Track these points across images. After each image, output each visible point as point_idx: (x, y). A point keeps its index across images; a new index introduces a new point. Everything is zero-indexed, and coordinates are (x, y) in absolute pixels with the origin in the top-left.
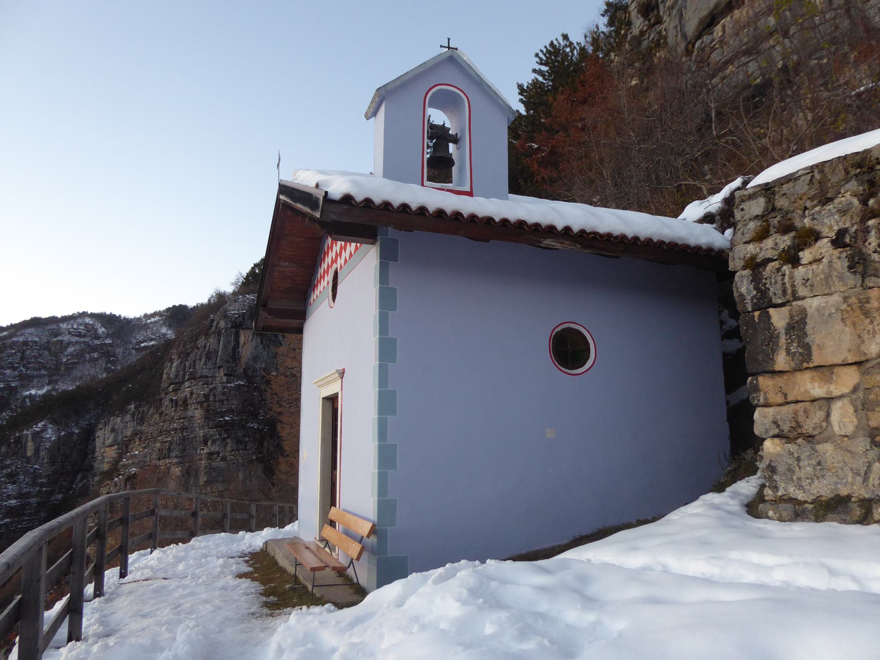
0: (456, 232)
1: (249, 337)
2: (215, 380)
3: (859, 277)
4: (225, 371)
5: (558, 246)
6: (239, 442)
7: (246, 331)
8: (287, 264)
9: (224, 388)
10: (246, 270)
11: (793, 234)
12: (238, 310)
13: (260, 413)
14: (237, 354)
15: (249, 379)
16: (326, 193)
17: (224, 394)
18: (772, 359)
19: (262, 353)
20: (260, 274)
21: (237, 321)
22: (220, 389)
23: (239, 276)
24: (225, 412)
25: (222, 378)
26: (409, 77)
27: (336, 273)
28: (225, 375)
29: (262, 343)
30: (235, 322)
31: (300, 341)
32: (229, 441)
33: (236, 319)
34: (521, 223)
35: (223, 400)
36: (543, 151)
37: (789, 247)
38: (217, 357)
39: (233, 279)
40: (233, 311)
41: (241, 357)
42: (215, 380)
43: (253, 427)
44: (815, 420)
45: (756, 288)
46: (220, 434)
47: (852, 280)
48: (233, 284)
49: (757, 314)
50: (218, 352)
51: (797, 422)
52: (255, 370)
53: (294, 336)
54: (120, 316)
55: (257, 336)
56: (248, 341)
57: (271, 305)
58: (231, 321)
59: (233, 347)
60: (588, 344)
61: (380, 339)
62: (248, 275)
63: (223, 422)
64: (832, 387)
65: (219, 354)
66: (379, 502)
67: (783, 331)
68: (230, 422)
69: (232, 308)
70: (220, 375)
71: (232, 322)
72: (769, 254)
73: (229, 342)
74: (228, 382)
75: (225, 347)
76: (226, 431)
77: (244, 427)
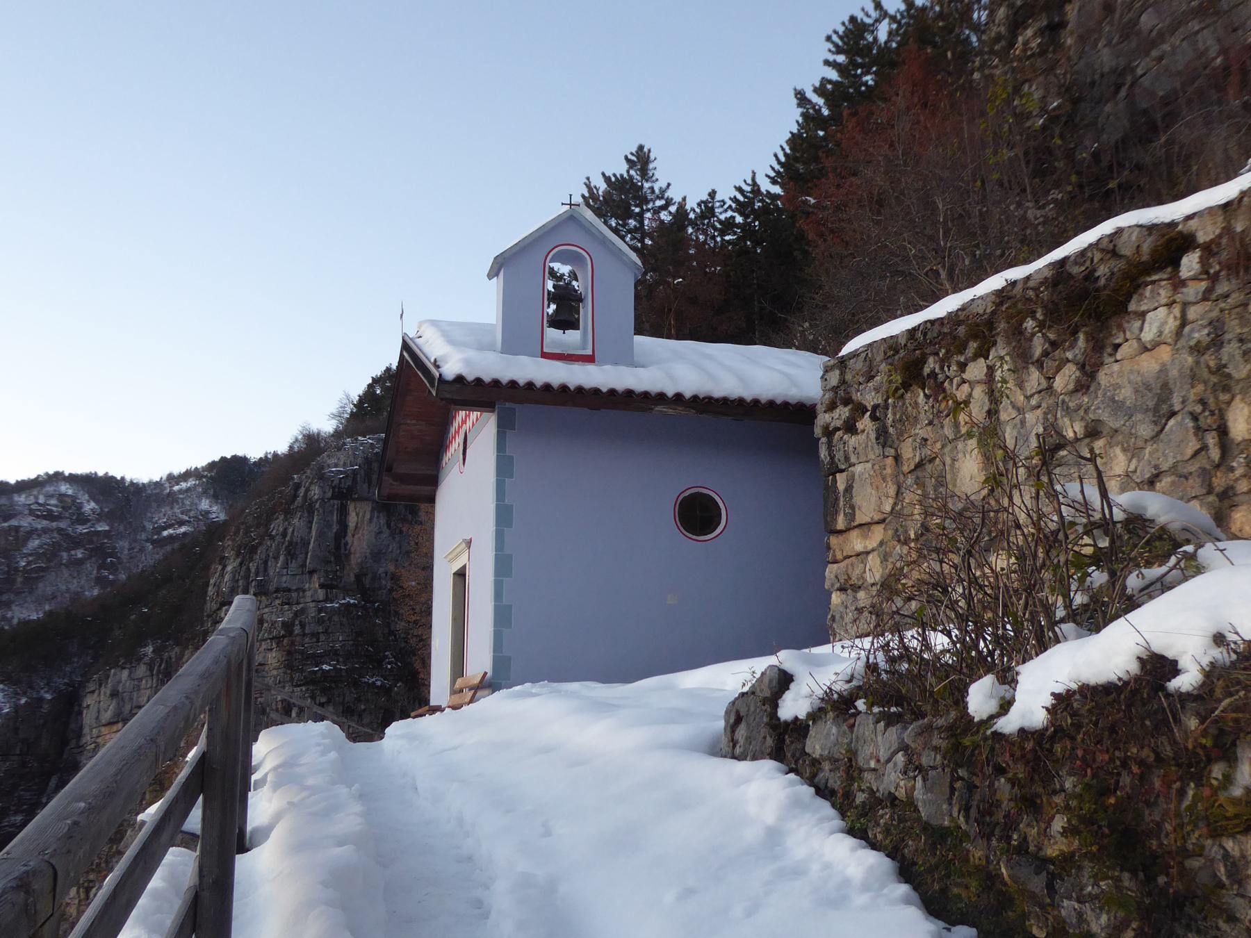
4: (322, 580)
5: (671, 411)
7: (359, 504)
8: (414, 422)
9: (320, 611)
10: (357, 389)
11: (850, 407)
12: (345, 465)
13: (386, 657)
14: (342, 545)
17: (320, 621)
18: (836, 520)
20: (383, 396)
21: (342, 486)
22: (312, 612)
24: (321, 656)
25: (316, 591)
28: (322, 586)
29: (389, 526)
30: (339, 488)
34: (629, 393)
35: (318, 633)
38: (307, 554)
39: (334, 407)
40: (336, 466)
41: (350, 553)
42: (304, 597)
43: (374, 683)
44: (857, 572)
45: (830, 455)
47: (878, 450)
48: (334, 416)
49: (831, 477)
51: (848, 575)
54: (123, 478)
55: (379, 512)
59: (336, 533)
62: (362, 399)
63: (319, 675)
64: (867, 542)
67: (842, 493)
68: (333, 674)
71: (334, 488)
72: (839, 423)
73: (328, 525)
74: (327, 600)
75: (321, 534)
77: (356, 684)
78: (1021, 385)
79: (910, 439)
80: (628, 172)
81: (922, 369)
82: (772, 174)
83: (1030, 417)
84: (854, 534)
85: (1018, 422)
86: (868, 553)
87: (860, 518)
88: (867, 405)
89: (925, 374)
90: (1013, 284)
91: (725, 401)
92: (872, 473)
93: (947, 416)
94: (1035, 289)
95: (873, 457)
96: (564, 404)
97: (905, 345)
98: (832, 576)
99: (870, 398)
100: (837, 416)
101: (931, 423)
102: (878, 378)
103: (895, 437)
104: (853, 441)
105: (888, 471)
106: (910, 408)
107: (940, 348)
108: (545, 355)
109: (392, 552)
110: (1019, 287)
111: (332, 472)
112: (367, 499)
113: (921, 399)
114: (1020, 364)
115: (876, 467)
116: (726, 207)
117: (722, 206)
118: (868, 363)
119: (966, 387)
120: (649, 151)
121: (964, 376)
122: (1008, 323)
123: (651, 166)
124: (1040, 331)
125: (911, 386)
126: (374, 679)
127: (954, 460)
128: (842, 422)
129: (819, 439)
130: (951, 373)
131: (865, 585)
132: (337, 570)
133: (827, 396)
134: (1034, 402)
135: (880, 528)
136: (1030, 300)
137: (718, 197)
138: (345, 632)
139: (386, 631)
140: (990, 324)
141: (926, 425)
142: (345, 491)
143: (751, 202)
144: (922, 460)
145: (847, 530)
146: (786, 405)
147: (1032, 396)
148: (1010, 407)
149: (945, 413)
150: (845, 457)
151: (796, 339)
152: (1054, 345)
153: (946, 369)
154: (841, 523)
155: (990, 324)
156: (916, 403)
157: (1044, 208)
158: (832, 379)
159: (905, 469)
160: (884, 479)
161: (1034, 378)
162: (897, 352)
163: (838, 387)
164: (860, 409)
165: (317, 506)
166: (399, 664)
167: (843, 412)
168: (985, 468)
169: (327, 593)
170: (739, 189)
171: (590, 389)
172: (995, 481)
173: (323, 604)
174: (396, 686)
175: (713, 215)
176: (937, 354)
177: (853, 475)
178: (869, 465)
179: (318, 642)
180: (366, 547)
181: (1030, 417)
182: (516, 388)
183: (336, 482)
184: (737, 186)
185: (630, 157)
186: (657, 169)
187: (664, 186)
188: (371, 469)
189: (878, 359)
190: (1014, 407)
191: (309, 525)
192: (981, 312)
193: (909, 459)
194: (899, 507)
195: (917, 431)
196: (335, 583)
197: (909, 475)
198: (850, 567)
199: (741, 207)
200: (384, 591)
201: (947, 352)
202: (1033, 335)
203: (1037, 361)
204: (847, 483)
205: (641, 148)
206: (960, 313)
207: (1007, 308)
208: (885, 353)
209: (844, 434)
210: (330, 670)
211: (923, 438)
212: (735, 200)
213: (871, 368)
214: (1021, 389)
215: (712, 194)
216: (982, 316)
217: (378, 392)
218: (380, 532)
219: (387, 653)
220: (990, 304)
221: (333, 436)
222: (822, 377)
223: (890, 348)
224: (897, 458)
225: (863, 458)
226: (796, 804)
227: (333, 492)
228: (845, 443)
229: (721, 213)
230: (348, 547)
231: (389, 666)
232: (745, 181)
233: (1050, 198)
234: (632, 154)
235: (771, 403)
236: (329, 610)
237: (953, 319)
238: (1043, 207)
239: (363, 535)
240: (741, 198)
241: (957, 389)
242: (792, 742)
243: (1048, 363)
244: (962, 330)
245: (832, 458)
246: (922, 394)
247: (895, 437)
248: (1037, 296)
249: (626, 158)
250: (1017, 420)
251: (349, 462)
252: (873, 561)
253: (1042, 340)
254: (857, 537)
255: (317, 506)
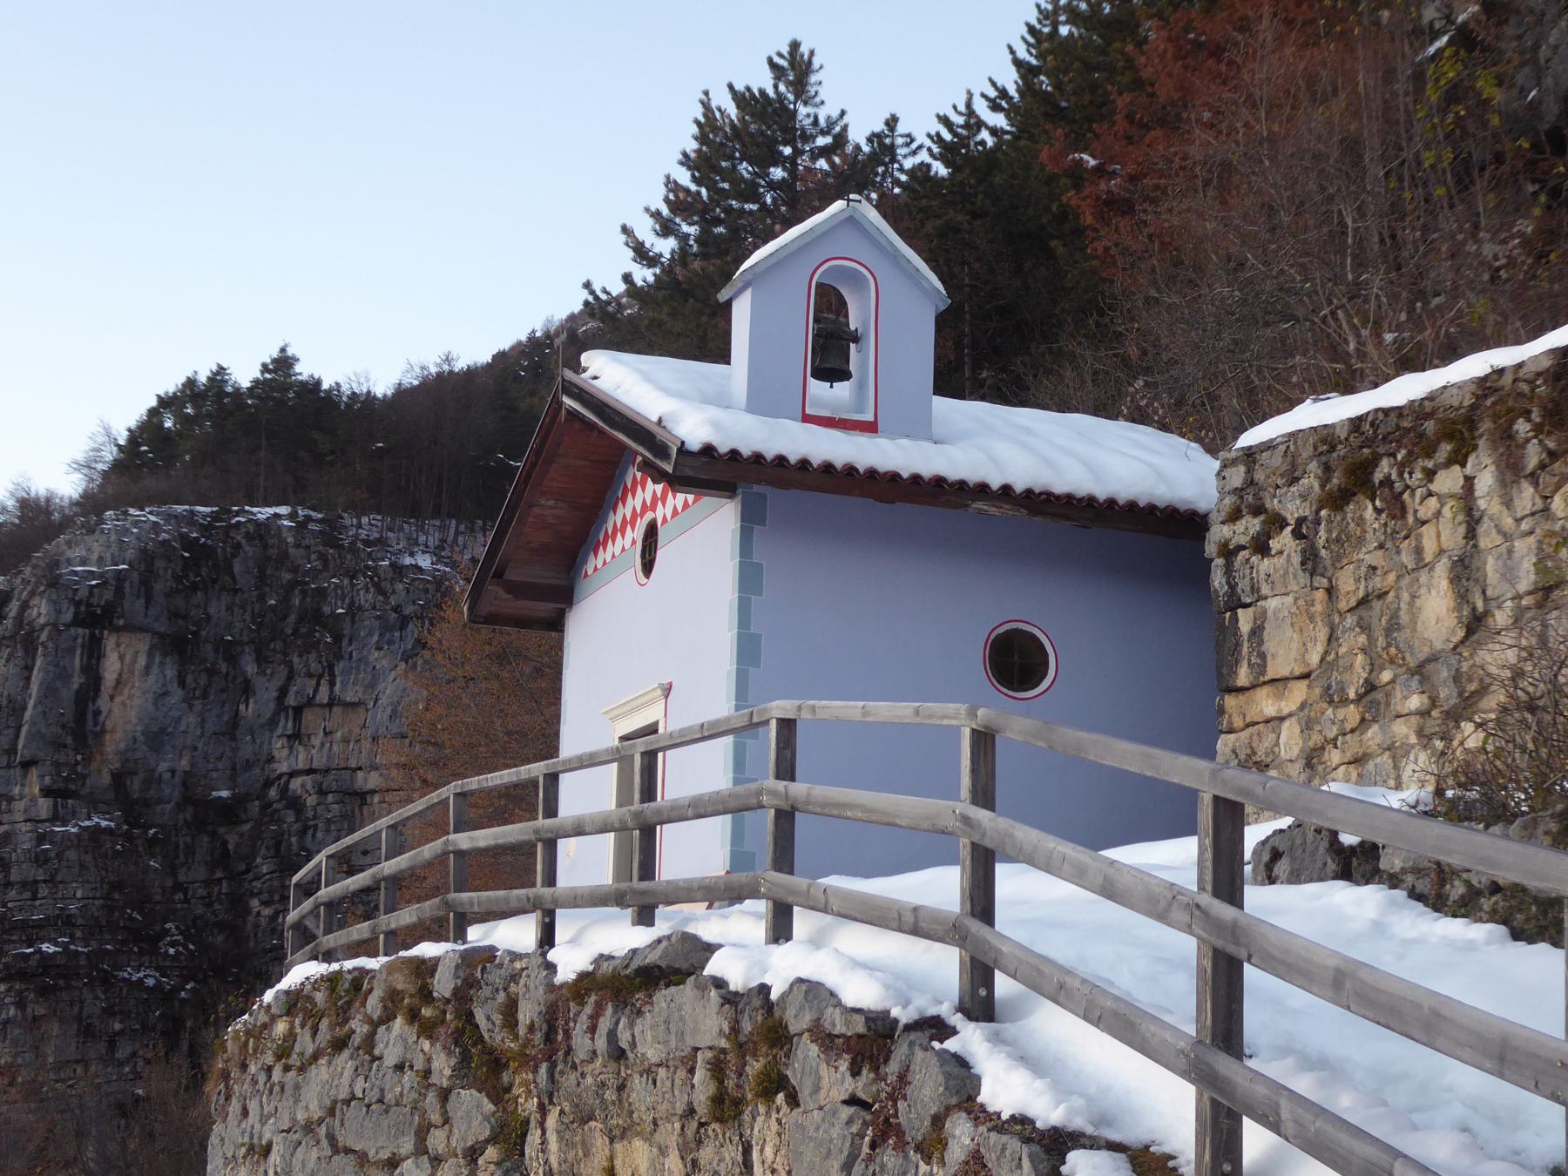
0: (848, 492)
1: (134, 661)
2: (9, 811)
3: (1308, 575)
4: (47, 780)
5: (993, 511)
6: (87, 1032)
7: (125, 638)
8: (551, 503)
9: (41, 839)
10: (127, 415)
11: (1262, 518)
12: (101, 561)
13: (167, 932)
14: (90, 716)
15: (133, 811)
16: (683, 443)
17: (40, 860)
18: (1235, 672)
19: (179, 720)
20: (179, 433)
21: (94, 601)
22: (25, 841)
23: (101, 439)
24: (39, 925)
25: (33, 800)
26: (787, 251)
27: (651, 532)
28: (46, 792)
29: (182, 683)
30: (89, 605)
31: (557, 650)
32: (55, 1028)
33: (91, 594)
34: (939, 481)
35: (36, 882)
36: (1113, 174)
37: (1258, 533)
38: (18, 728)
39: (79, 449)
40: (84, 562)
41: (103, 731)
42: (9, 811)
43: (141, 981)
44: (1266, 744)
45: (1228, 583)
46: (21, 1004)
47: (1303, 579)
48: (79, 466)
49: (1228, 614)
50: (24, 708)
51: (1252, 749)
52: (152, 779)
53: (534, 637)
55: (165, 655)
56: (132, 672)
57: (512, 575)
58: (72, 600)
59: (77, 692)
60: (1046, 655)
61: (739, 634)
62: (135, 437)
63: (33, 962)
64: (1283, 704)
65: (28, 715)
66: (733, 853)
67: (1246, 637)
68: (61, 961)
69: (77, 553)
70: (27, 790)
71: (78, 604)
72: (1243, 540)
73: (64, 675)
74: (55, 818)
75: (49, 692)
76: (44, 992)
77: (107, 981)
78: (1508, 503)
79: (1352, 566)
80: (776, 87)
81: (1372, 473)
82: (993, 93)
83: (1520, 546)
84: (1263, 692)
85: (1505, 551)
86: (1282, 719)
87: (1275, 669)
88: (1289, 517)
89: (1377, 481)
90: (1500, 372)
91: (1069, 499)
92: (1294, 610)
93: (1406, 538)
94: (1531, 382)
95: (1296, 588)
96: (849, 493)
97: (1346, 439)
98: (1228, 750)
99: (1292, 506)
100: (1242, 530)
101: (1381, 546)
102: (1304, 481)
103: (1328, 563)
104: (1265, 565)
105: (1318, 608)
106: (1352, 525)
107: (1400, 447)
108: (807, 419)
109: (185, 732)
110: (1507, 379)
111: (76, 574)
112: (142, 629)
113: (1369, 513)
114: (1509, 477)
115: (1301, 602)
116: (914, 146)
117: (908, 145)
118: (1289, 459)
119: (1433, 502)
120: (812, 53)
121: (1432, 487)
122: (1495, 422)
123: (813, 78)
124: (1535, 437)
125: (1355, 494)
126: (141, 975)
127: (1414, 597)
128: (1248, 538)
129: (1212, 560)
130: (1413, 482)
131: (1277, 762)
132: (77, 763)
133: (1227, 501)
134: (1524, 526)
135: (1303, 684)
136: (1521, 395)
137: (901, 128)
138: (88, 882)
139: (169, 883)
140: (1470, 421)
141: (1375, 548)
142: (99, 612)
143: (963, 141)
144: (1368, 595)
145: (1253, 687)
146: (1152, 508)
147: (1522, 518)
148: (1494, 531)
149: (1403, 534)
150: (1252, 588)
151: (1125, 405)
152: (1553, 455)
153: (1406, 476)
154: (1243, 676)
155: (1470, 421)
156: (1361, 518)
157: (1507, 243)
158: (1234, 477)
159: (1343, 605)
160: (1311, 618)
161: (1526, 497)
162: (1333, 448)
163: (1242, 489)
164: (1278, 522)
165: (44, 636)
166: (191, 947)
167: (1251, 525)
168: (1458, 608)
169: (55, 806)
170: (945, 121)
171: (886, 473)
172: (1475, 625)
173: (46, 827)
174: (184, 989)
175: (894, 160)
176: (1394, 455)
177: (1264, 612)
178: (1290, 599)
179: (34, 898)
180: (135, 720)
181: (1520, 546)
182: (784, 466)
183: (83, 594)
184: (941, 114)
185: (777, 60)
186: (824, 84)
187: (835, 114)
188: (151, 571)
189: (1305, 455)
190: (1499, 532)
191: (26, 674)
192: (1456, 404)
193: (1348, 593)
194: (1332, 656)
195: (1361, 556)
196: (73, 787)
197: (1349, 615)
198: (1255, 737)
199: (948, 152)
200: (169, 807)
201: (1410, 453)
202: (1528, 441)
203: (1532, 474)
204: (1255, 623)
205: (795, 46)
206: (1426, 403)
207: (1494, 404)
208: (1315, 448)
209: (1252, 555)
210: (55, 952)
211: (1370, 566)
212: (938, 139)
213: (1294, 466)
214: (1508, 509)
215: (892, 122)
216: (1457, 409)
217: (168, 424)
218: (166, 694)
219: (168, 926)
220: (1468, 396)
221: (77, 504)
222: (1218, 474)
223: (1324, 441)
224: (1330, 591)
225: (1279, 589)
226: (1393, 903)
227: (76, 614)
228: (1252, 568)
229: (905, 157)
230: (102, 718)
231: (172, 951)
232: (955, 107)
233: (1515, 230)
234: (780, 55)
235: (1132, 506)
236: (58, 839)
237: (1419, 410)
238: (1504, 242)
239: (130, 697)
240: (947, 136)
241: (1421, 503)
242: (1359, 864)
243: (1544, 478)
244: (1430, 426)
245: (1232, 587)
246: (1370, 507)
247: (1328, 563)
248: (1533, 390)
249: (770, 61)
250: (1503, 549)
251: (108, 555)
252: (1290, 731)
253: (1538, 449)
254: (1268, 696)
255: (44, 636)
